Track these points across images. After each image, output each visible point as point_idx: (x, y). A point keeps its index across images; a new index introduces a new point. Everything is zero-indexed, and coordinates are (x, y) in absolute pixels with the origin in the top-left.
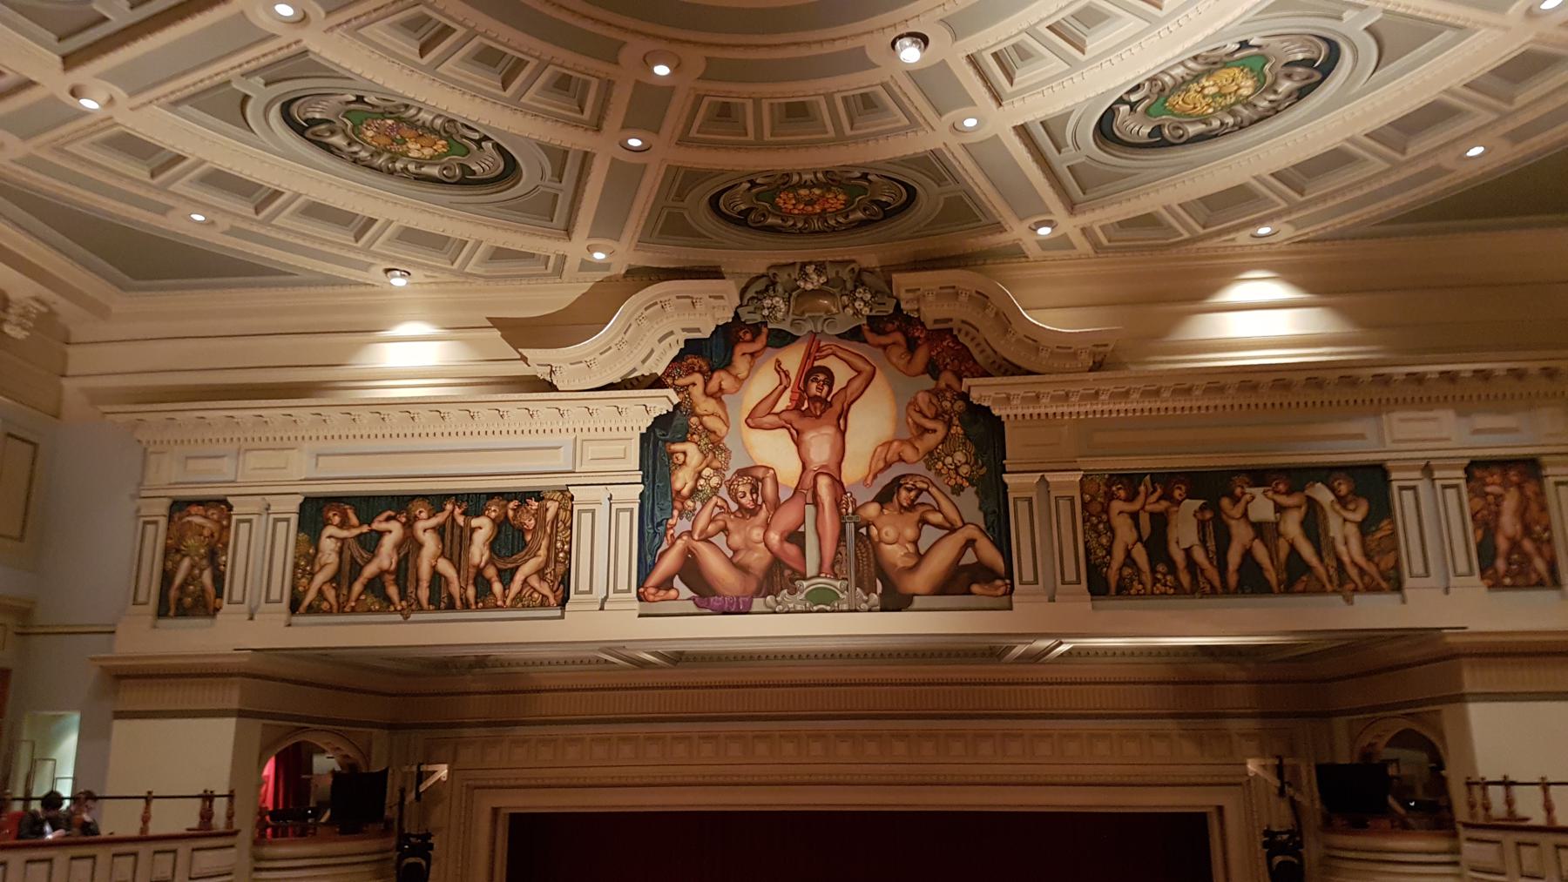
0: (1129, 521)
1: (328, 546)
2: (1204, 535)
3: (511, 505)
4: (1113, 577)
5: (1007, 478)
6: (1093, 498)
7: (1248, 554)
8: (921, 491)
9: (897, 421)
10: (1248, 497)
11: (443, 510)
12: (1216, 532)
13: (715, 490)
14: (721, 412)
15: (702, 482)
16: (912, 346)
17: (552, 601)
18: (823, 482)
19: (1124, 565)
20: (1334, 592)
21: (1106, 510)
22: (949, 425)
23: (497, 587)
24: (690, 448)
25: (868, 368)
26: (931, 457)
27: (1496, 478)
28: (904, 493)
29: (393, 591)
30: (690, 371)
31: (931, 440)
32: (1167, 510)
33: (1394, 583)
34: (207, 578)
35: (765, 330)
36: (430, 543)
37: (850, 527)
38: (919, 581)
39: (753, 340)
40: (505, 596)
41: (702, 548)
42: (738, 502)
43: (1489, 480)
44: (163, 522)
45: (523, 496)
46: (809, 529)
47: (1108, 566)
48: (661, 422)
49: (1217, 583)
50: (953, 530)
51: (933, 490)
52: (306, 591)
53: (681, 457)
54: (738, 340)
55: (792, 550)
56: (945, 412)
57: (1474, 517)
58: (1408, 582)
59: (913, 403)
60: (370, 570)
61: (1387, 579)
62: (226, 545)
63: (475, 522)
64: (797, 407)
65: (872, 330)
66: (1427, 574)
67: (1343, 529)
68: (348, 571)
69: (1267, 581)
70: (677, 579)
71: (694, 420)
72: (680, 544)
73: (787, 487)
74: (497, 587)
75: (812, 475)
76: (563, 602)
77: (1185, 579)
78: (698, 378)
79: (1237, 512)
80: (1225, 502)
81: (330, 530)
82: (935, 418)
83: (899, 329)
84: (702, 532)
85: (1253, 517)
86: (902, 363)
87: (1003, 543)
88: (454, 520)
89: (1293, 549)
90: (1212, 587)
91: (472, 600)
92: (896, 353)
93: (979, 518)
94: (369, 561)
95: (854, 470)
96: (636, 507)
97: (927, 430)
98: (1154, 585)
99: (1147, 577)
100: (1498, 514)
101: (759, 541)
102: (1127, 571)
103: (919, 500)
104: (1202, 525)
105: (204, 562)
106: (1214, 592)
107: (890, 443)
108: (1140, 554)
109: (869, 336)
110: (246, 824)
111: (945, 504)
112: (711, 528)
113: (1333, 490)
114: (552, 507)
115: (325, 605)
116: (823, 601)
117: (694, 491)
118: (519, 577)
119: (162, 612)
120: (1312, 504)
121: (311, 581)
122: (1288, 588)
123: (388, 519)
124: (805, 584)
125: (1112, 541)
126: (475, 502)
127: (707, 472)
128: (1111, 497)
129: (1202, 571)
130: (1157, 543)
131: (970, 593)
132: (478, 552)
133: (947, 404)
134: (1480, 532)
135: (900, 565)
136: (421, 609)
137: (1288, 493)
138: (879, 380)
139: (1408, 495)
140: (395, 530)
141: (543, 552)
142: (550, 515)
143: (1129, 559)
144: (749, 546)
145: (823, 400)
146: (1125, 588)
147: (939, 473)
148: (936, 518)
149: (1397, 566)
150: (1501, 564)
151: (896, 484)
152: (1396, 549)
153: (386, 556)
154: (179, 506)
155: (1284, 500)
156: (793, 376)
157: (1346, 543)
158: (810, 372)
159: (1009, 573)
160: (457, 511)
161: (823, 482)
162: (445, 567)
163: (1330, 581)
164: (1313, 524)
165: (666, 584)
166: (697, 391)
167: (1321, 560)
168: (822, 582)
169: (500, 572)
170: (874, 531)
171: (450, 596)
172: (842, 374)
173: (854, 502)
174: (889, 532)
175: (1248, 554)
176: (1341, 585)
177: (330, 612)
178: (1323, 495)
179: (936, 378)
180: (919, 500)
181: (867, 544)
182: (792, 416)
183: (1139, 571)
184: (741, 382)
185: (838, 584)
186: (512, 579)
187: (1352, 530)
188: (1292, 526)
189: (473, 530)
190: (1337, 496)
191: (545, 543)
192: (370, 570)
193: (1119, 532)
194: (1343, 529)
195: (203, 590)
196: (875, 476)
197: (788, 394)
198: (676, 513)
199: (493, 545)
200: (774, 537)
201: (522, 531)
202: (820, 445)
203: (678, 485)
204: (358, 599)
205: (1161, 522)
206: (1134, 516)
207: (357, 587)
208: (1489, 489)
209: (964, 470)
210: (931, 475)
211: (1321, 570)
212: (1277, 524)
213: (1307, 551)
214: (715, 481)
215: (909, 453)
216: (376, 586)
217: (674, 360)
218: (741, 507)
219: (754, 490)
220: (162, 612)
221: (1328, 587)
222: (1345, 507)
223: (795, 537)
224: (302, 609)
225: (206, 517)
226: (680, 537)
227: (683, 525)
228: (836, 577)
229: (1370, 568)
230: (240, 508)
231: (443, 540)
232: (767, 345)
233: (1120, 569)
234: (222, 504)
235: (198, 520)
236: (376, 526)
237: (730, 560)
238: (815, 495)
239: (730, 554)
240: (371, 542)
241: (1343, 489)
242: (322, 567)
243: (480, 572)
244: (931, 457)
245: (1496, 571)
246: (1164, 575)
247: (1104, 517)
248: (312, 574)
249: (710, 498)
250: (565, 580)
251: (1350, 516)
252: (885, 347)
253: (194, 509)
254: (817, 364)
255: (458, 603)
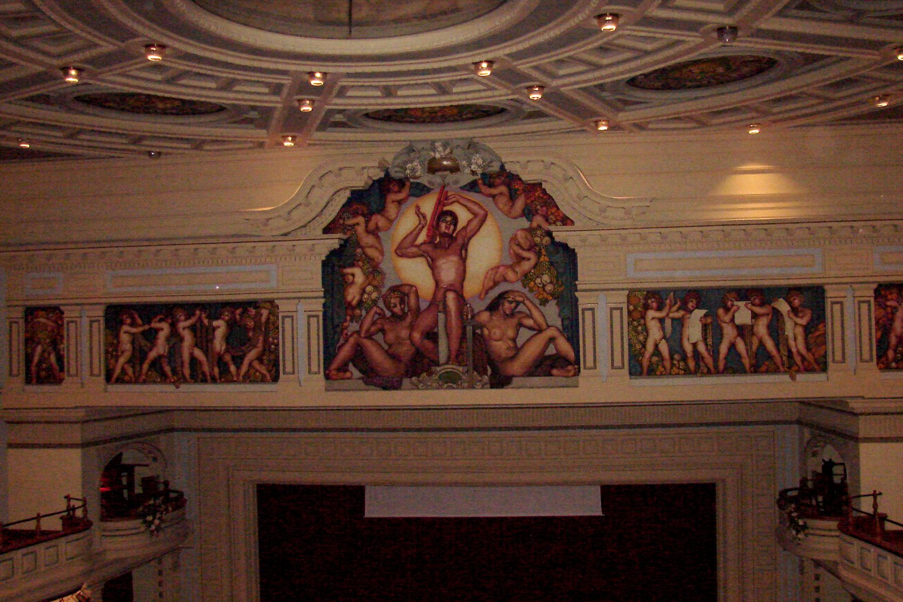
0: (658, 325)
1: (125, 338)
2: (706, 335)
3: (238, 311)
4: (645, 363)
5: (577, 294)
6: (635, 309)
7: (733, 346)
8: (518, 303)
9: (501, 250)
10: (735, 308)
11: (194, 315)
12: (712, 330)
13: (375, 302)
14: (378, 245)
15: (366, 296)
16: (512, 198)
17: (268, 377)
18: (451, 296)
19: (653, 355)
20: (785, 372)
21: (643, 317)
22: (539, 254)
23: (233, 368)
24: (357, 271)
25: (482, 212)
26: (526, 278)
27: (894, 296)
28: (507, 305)
29: (167, 369)
30: (355, 214)
31: (526, 266)
32: (683, 316)
33: (822, 366)
34: (53, 359)
35: (408, 184)
36: (188, 338)
37: (469, 329)
38: (516, 367)
39: (400, 191)
40: (238, 374)
41: (368, 343)
42: (392, 311)
43: (889, 297)
44: (22, 322)
45: (245, 305)
46: (441, 329)
47: (643, 355)
48: (333, 253)
49: (711, 367)
50: (540, 331)
51: (527, 302)
52: (114, 367)
53: (351, 277)
54: (389, 191)
55: (428, 344)
56: (536, 245)
57: (877, 323)
58: (831, 366)
59: (514, 239)
60: (153, 355)
61: (818, 364)
62: (62, 337)
63: (215, 323)
64: (430, 241)
65: (484, 184)
66: (844, 360)
67: (793, 329)
68: (139, 356)
69: (743, 364)
70: (351, 365)
71: (359, 250)
72: (352, 340)
73: (426, 300)
74: (233, 368)
75: (442, 290)
76: (275, 379)
77: (691, 364)
78: (361, 219)
79: (727, 318)
80: (721, 311)
81: (125, 328)
82: (529, 250)
83: (503, 183)
84: (367, 331)
85: (738, 321)
86: (506, 208)
87: (573, 340)
88: (202, 322)
89: (762, 344)
90: (709, 369)
91: (217, 376)
92: (502, 200)
93: (559, 323)
94: (151, 350)
95: (472, 287)
96: (321, 314)
97: (524, 259)
98: (671, 368)
99: (667, 364)
100: (892, 320)
101: (406, 338)
102: (655, 359)
103: (518, 310)
104: (705, 327)
105: (50, 348)
106: (709, 373)
107: (498, 267)
108: (664, 348)
109: (484, 189)
110: (94, 513)
111: (535, 313)
112: (373, 329)
113: (790, 303)
114: (265, 313)
115: (127, 378)
116: (451, 380)
117: (360, 303)
118: (246, 362)
119: (28, 381)
120: (776, 313)
121: (117, 361)
122: (756, 369)
123: (160, 321)
124: (438, 369)
125: (646, 339)
126: (214, 309)
127: (369, 289)
128: (647, 307)
129: (703, 358)
130: (675, 338)
131: (550, 375)
132: (219, 344)
133: (537, 240)
134: (879, 333)
135: (504, 355)
136: (185, 381)
137: (762, 305)
138: (489, 222)
139: (837, 307)
140: (165, 329)
141: (260, 345)
142: (264, 319)
143: (657, 351)
144: (399, 341)
145: (450, 236)
146: (653, 370)
147: (531, 290)
148: (529, 322)
149: (825, 356)
150: (891, 354)
151: (502, 296)
152: (825, 343)
153: (161, 347)
154: (31, 312)
155: (757, 310)
156: (429, 217)
157: (795, 340)
158: (442, 214)
159: (577, 362)
160: (204, 315)
161: (451, 296)
162: (198, 353)
163: (783, 365)
164: (776, 329)
165: (343, 368)
166: (361, 229)
167: (779, 351)
168: (450, 367)
169: (234, 359)
170: (486, 332)
171: (204, 374)
172: (463, 216)
173: (472, 310)
174: (497, 333)
175: (733, 346)
176: (789, 368)
177: (129, 382)
178: (783, 306)
179: (530, 220)
180: (518, 310)
181: (481, 341)
182: (429, 248)
183: (662, 359)
184: (391, 222)
185: (461, 369)
186: (242, 363)
187: (799, 330)
188: (761, 329)
189: (214, 329)
190: (792, 307)
191: (261, 338)
192: (153, 355)
193: (651, 332)
194: (793, 329)
195: (51, 365)
196: (487, 293)
197: (426, 228)
198: (348, 318)
199: (227, 338)
200: (417, 336)
201: (246, 329)
202: (448, 269)
203: (349, 298)
204: (146, 374)
205: (679, 324)
206: (661, 321)
207: (146, 366)
208: (889, 303)
209: (549, 288)
210: (526, 291)
211: (778, 359)
212: (752, 326)
213: (770, 345)
214: (374, 295)
215: (510, 275)
216: (156, 364)
217: (344, 206)
218: (394, 314)
219: (402, 302)
220: (28, 381)
221: (782, 369)
222: (796, 315)
223: (431, 336)
224: (113, 379)
225: (48, 318)
226: (351, 335)
227: (354, 327)
228: (460, 364)
229: (809, 356)
230: (69, 314)
231: (195, 336)
232: (409, 196)
233: (651, 357)
234: (56, 311)
235: (42, 320)
236: (155, 325)
237: (387, 352)
238: (445, 305)
239: (386, 347)
240: (151, 335)
241: (797, 302)
242: (123, 352)
243: (220, 358)
244: (526, 278)
245: (887, 359)
246: (678, 361)
247: (642, 321)
248: (117, 357)
249: (371, 308)
250: (276, 364)
251: (799, 321)
252: (493, 196)
253: (41, 313)
254: (446, 208)
255: (209, 377)
